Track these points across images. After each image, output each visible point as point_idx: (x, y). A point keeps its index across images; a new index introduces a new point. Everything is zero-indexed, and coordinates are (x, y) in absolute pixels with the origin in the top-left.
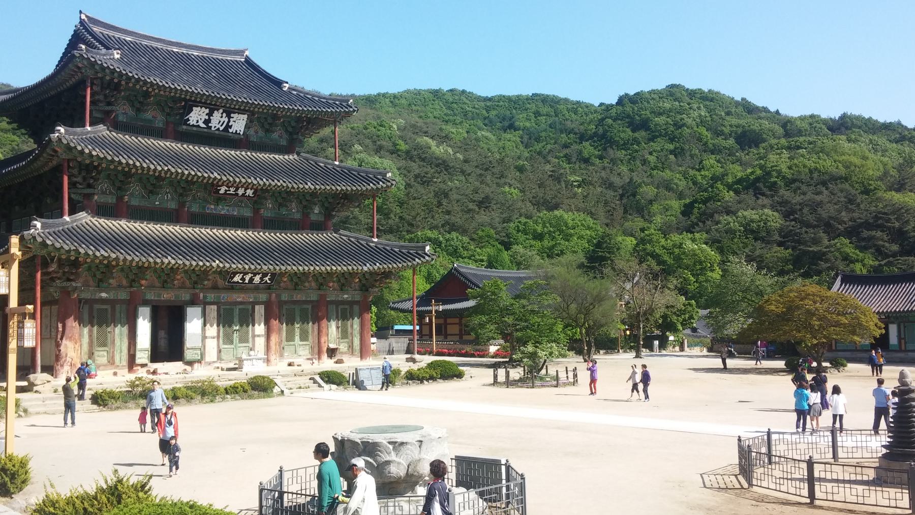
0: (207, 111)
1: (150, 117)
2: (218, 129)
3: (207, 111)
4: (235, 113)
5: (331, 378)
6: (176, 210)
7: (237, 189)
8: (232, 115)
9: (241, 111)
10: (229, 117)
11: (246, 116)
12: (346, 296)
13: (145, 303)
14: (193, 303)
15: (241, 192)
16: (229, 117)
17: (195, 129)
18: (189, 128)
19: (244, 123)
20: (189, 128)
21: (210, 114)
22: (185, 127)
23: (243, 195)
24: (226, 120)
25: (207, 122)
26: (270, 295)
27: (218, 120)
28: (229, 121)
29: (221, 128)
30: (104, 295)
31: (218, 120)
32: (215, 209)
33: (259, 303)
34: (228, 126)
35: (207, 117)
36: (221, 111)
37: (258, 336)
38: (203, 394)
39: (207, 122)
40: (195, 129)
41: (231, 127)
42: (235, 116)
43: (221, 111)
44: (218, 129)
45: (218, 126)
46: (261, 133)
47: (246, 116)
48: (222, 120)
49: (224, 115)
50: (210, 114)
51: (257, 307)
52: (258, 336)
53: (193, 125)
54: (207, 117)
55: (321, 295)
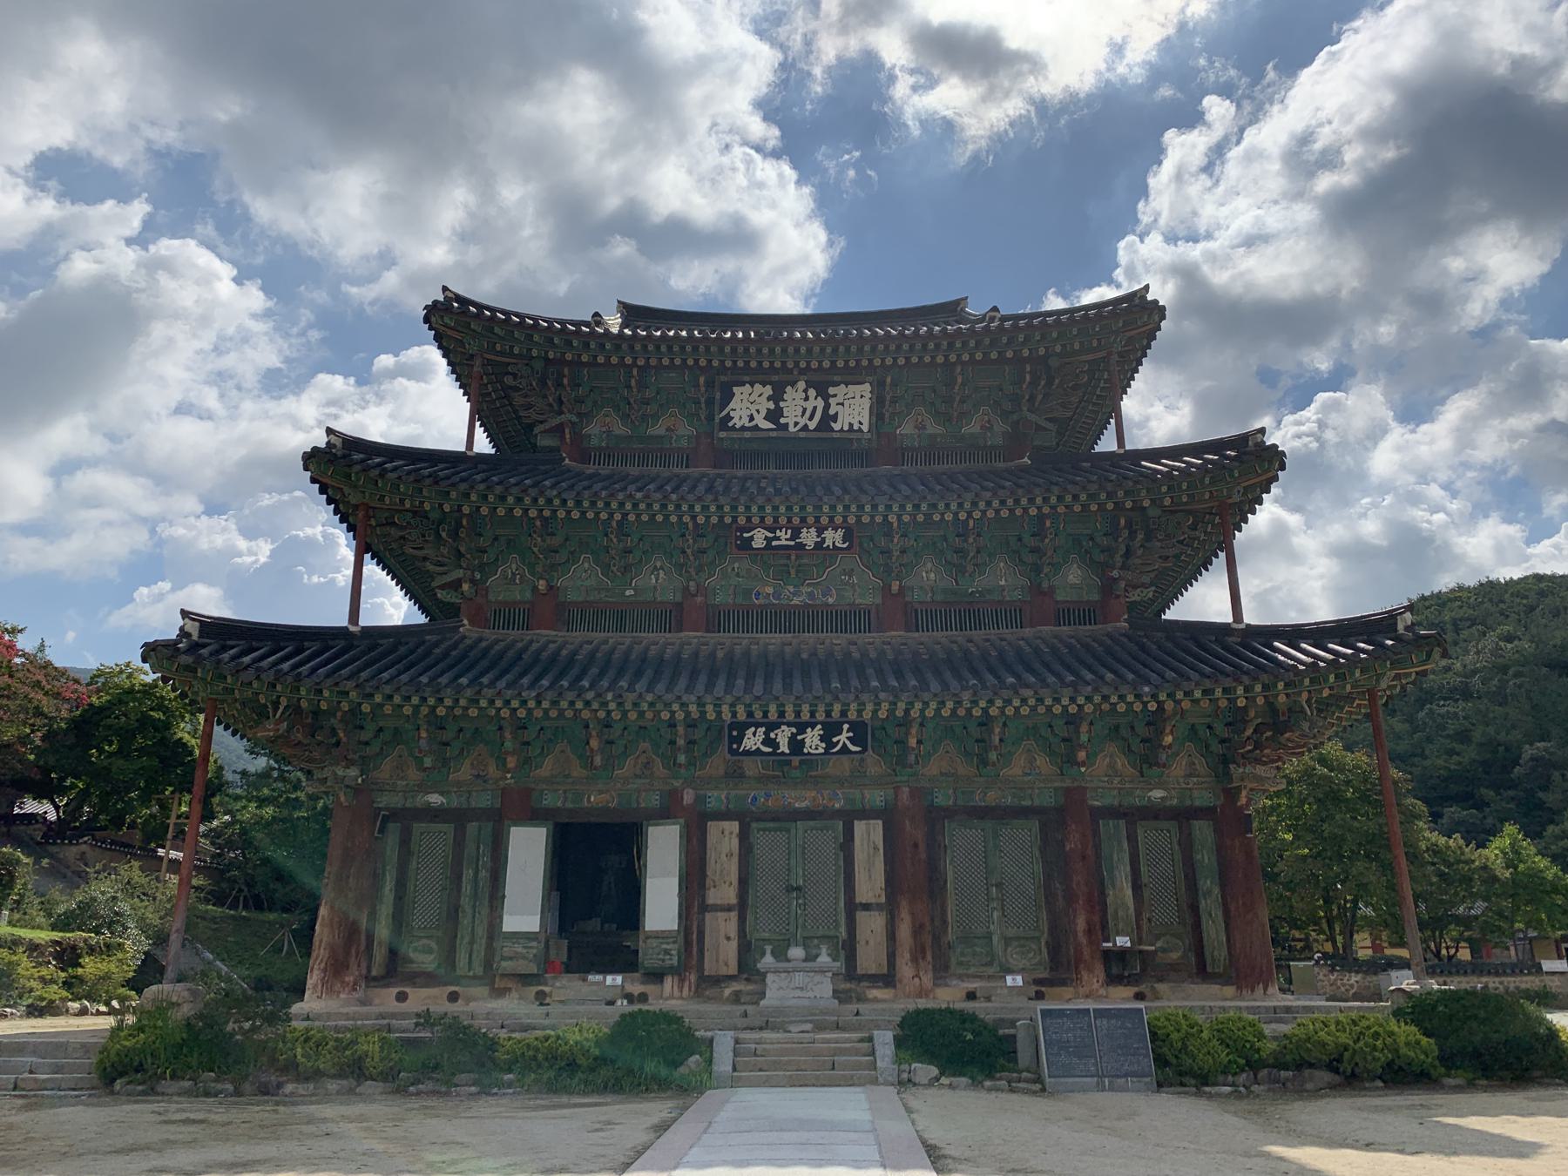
0: (768, 390)
1: (662, 432)
2: (805, 428)
3: (768, 390)
4: (836, 384)
5: (166, 1122)
6: (679, 605)
7: (796, 534)
8: (831, 391)
9: (852, 376)
10: (826, 397)
11: (867, 387)
12: (1157, 794)
13: (533, 816)
14: (664, 815)
15: (809, 538)
16: (826, 397)
17: (747, 435)
18: (735, 435)
19: (866, 403)
20: (735, 435)
21: (777, 397)
22: (723, 435)
23: (819, 545)
24: (820, 403)
25: (774, 415)
26: (897, 789)
27: (799, 408)
28: (827, 406)
29: (812, 425)
30: (435, 799)
31: (799, 408)
32: (777, 595)
33: (866, 814)
34: (828, 419)
35: (771, 406)
36: (801, 385)
37: (866, 907)
38: (572, 1066)
39: (774, 415)
40: (747, 435)
41: (835, 418)
42: (839, 391)
43: (801, 385)
44: (805, 428)
45: (802, 422)
46: (933, 428)
47: (867, 387)
48: (809, 406)
49: (812, 393)
50: (777, 397)
51: (859, 827)
52: (866, 907)
53: (743, 428)
54: (771, 406)
55: (1068, 791)
